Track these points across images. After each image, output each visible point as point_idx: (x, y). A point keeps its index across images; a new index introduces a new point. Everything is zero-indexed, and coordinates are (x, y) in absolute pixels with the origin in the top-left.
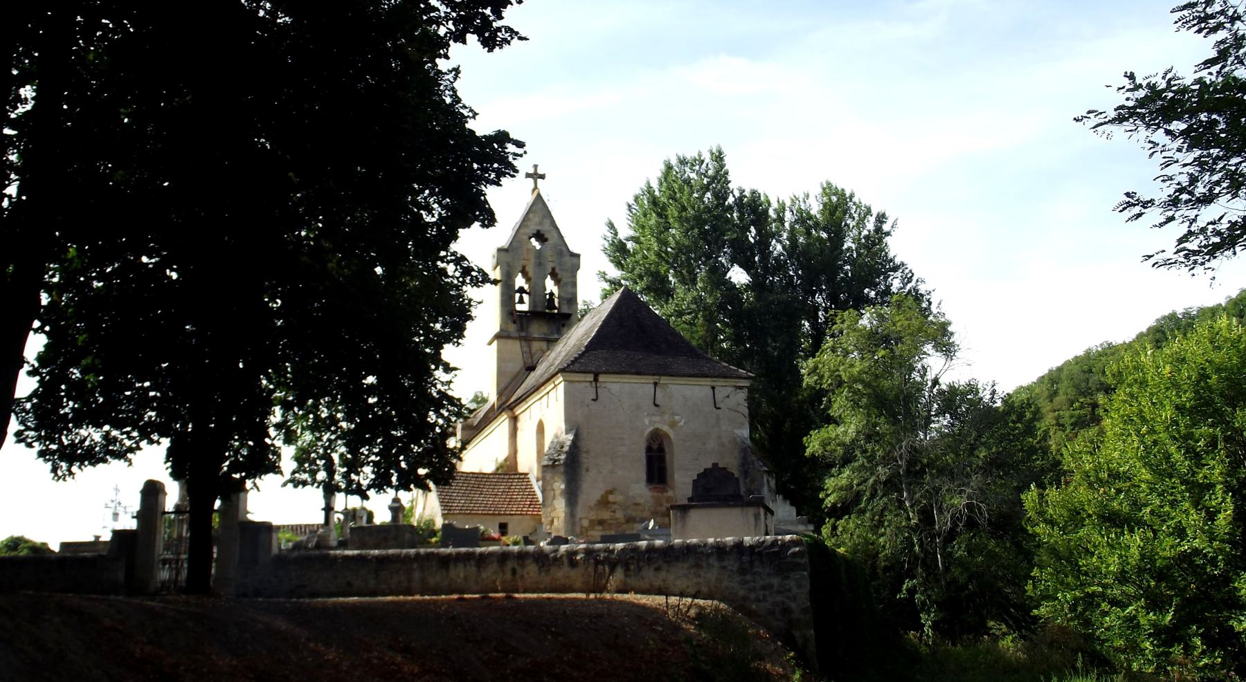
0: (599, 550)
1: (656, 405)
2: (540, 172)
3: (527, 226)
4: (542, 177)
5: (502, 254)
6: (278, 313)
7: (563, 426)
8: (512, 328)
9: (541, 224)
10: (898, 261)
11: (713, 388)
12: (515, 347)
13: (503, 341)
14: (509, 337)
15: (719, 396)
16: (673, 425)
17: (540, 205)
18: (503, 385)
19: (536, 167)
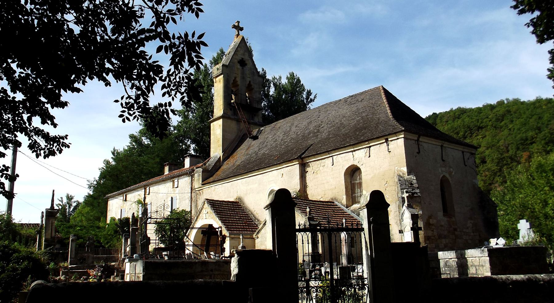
0: (32, 282)
1: (443, 160)
2: (241, 26)
3: (237, 55)
4: (234, 27)
5: (224, 67)
6: (19, 84)
7: (405, 169)
8: (230, 113)
9: (244, 55)
10: (149, 99)
11: (463, 152)
12: (233, 125)
13: (226, 120)
14: (229, 118)
15: (466, 158)
16: (450, 173)
17: (243, 44)
18: (225, 147)
19: (238, 22)
